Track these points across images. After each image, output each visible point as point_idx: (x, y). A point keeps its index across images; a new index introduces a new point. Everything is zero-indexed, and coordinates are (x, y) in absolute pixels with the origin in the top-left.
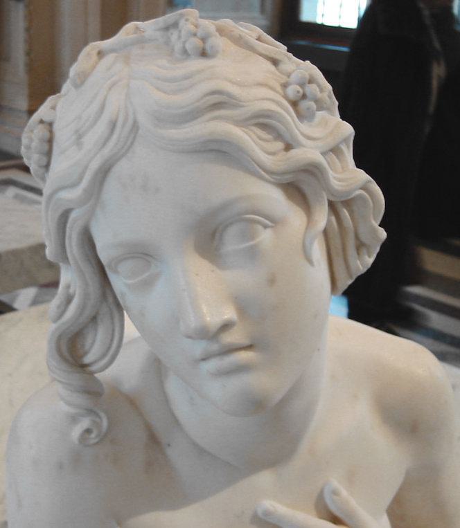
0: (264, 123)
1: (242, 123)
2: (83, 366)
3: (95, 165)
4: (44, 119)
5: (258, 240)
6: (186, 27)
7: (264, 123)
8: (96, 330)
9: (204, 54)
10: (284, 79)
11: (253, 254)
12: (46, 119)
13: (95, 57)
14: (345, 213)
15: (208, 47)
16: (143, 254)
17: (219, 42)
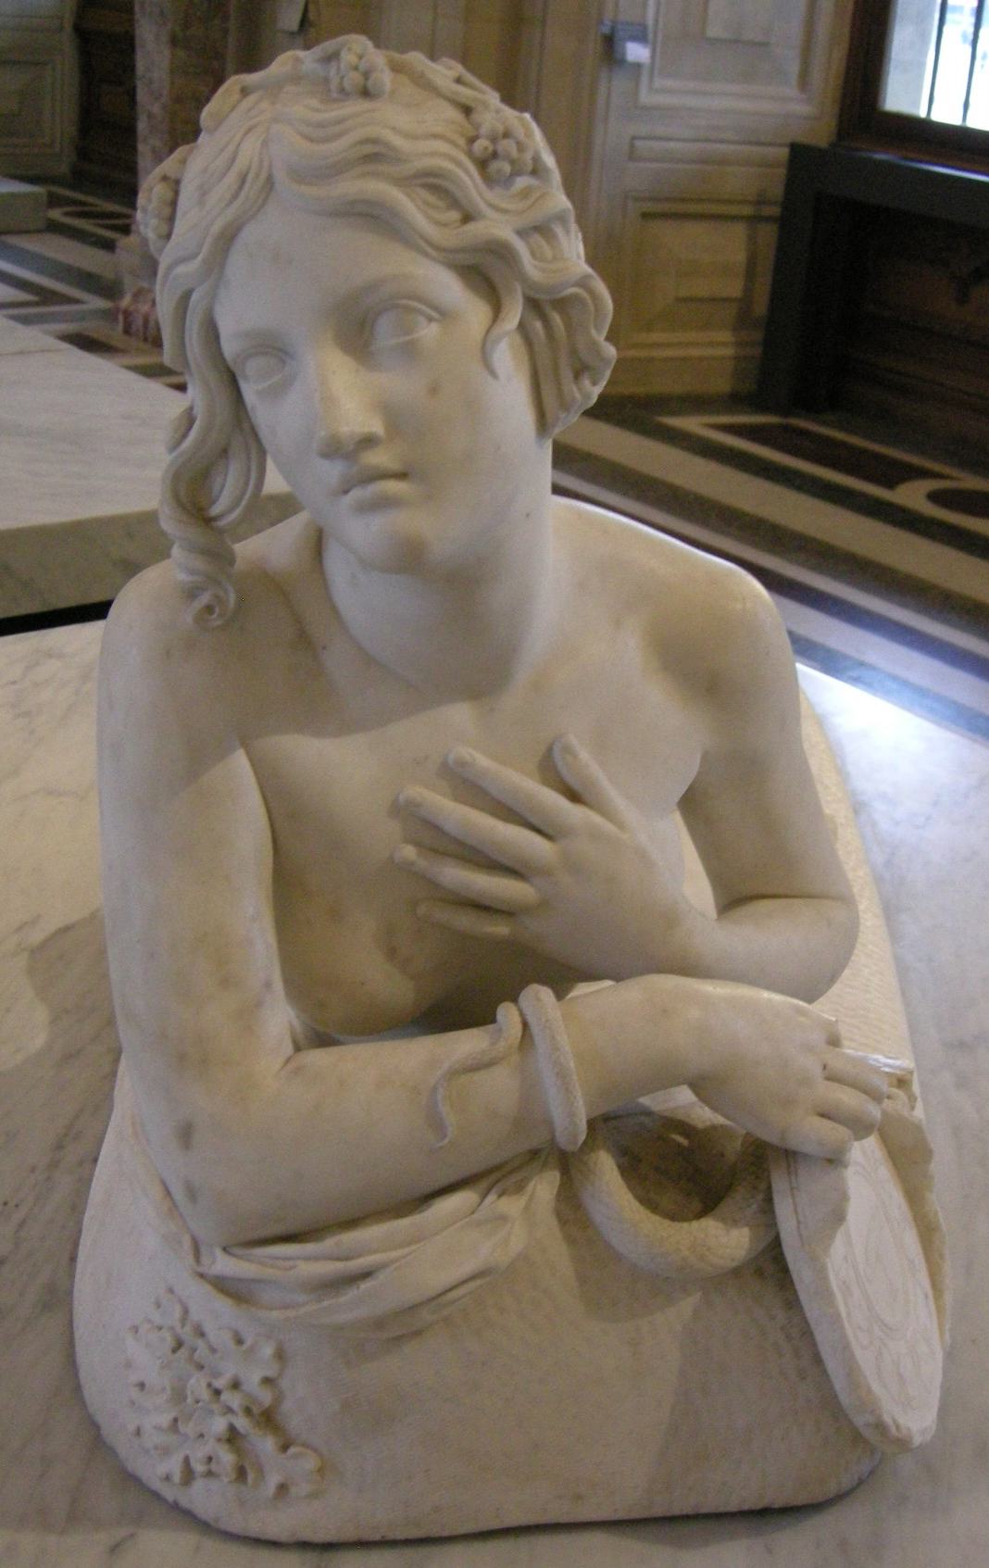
0: (434, 185)
1: (404, 182)
2: (208, 521)
3: (216, 228)
4: (168, 174)
5: (416, 336)
6: (348, 58)
7: (434, 185)
8: (227, 467)
9: (366, 93)
10: (472, 133)
11: (410, 352)
12: (173, 175)
13: (236, 96)
14: (556, 318)
15: (370, 83)
16: (274, 348)
17: (386, 78)
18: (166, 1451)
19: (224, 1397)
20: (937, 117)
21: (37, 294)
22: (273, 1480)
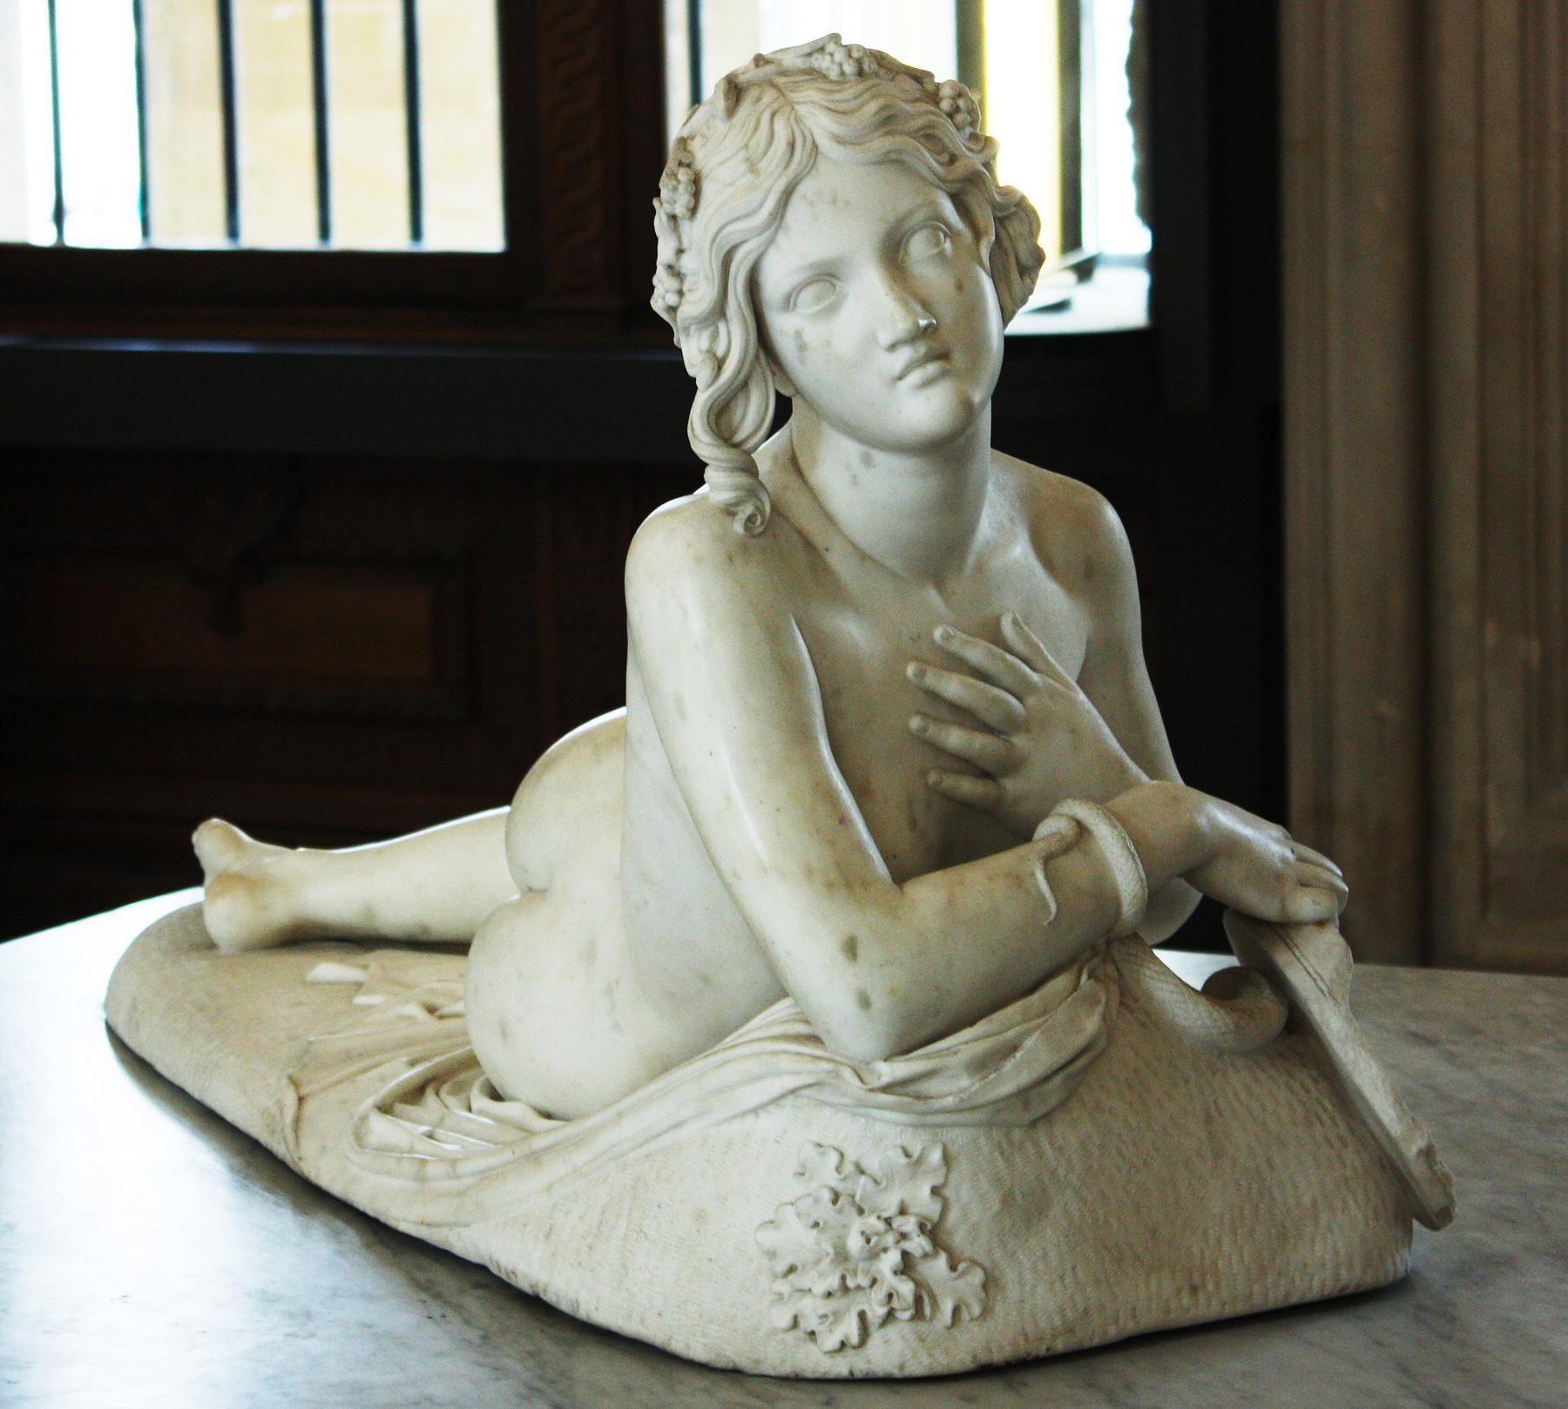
18: (837, 1316)
19: (895, 1225)
20: (80, 236)
21: (775, 219)
22: (947, 1307)
